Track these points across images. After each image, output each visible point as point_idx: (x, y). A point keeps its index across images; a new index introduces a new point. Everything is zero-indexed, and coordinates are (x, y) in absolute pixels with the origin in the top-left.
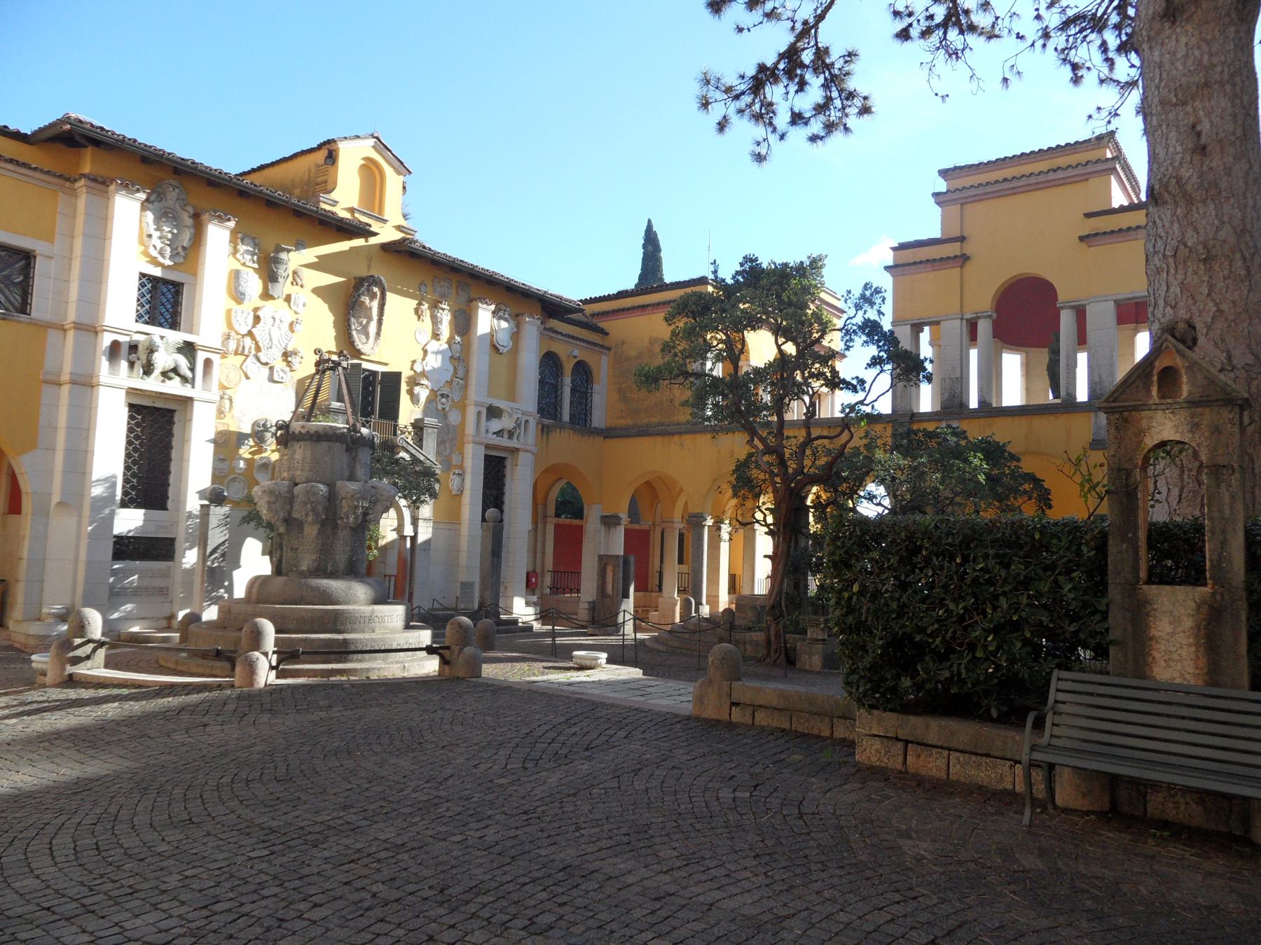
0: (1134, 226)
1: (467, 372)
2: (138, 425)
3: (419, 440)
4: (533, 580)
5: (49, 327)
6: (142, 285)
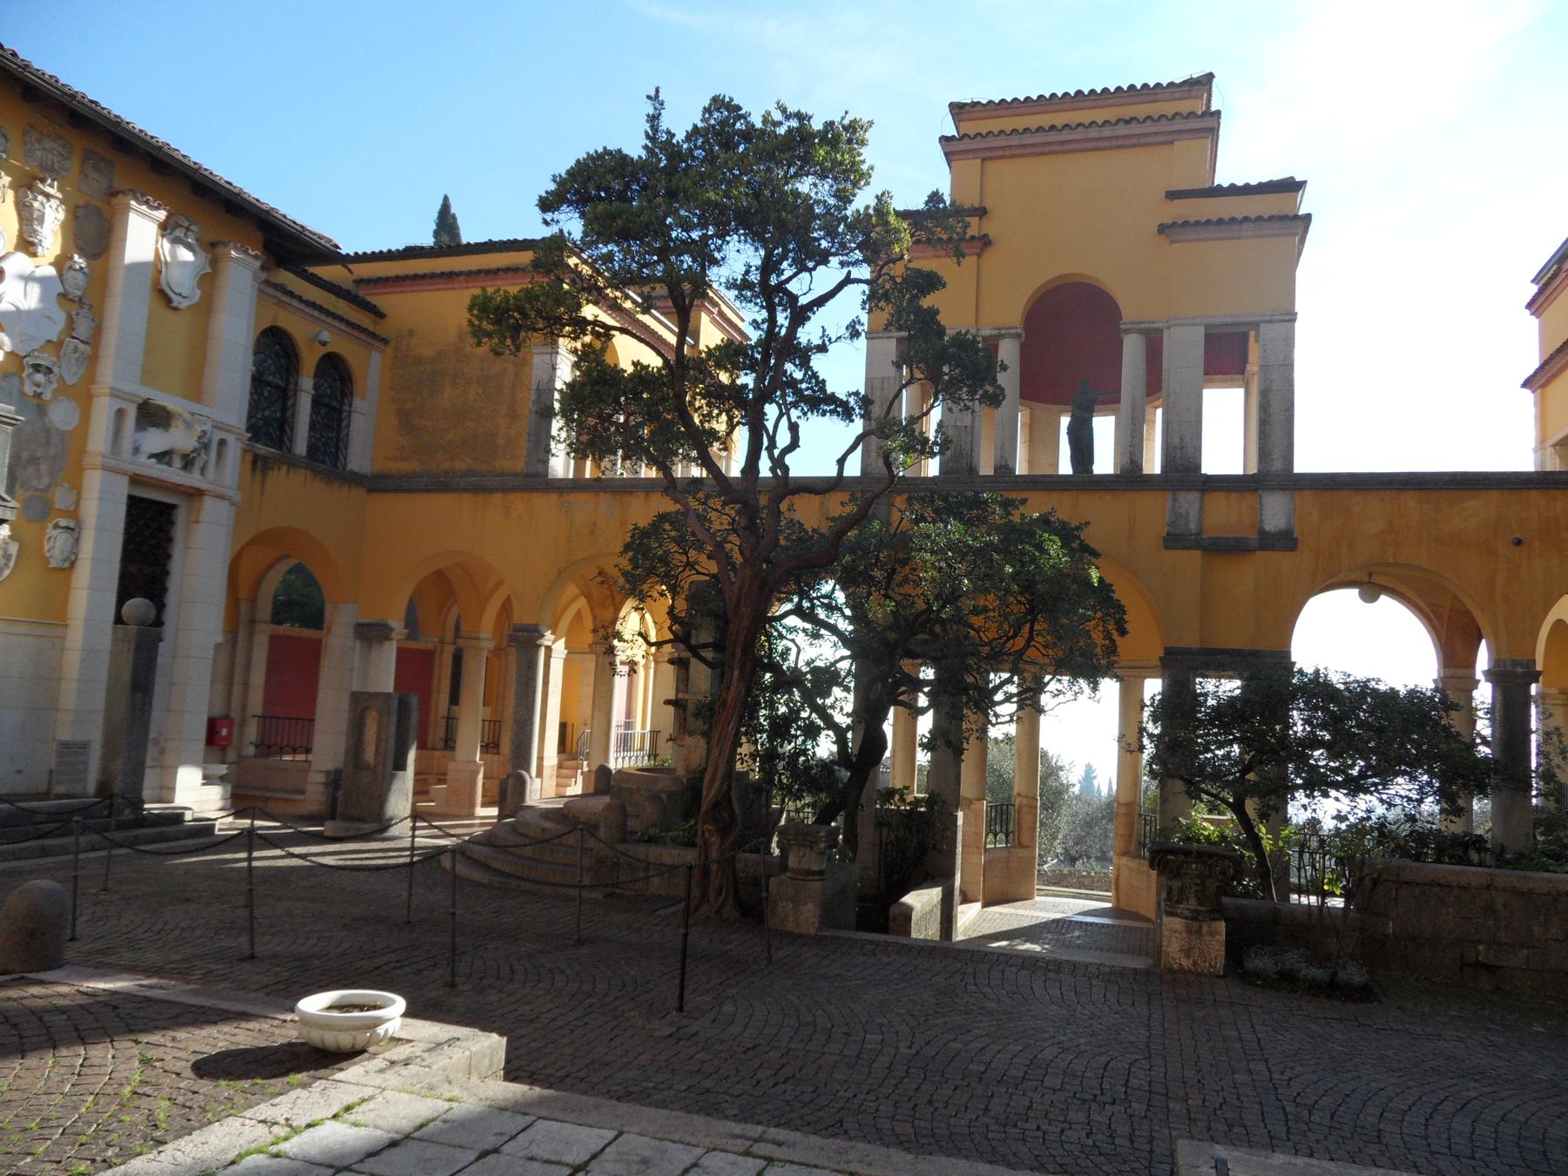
0: (1240, 216)
1: (98, 331)
4: (224, 732)
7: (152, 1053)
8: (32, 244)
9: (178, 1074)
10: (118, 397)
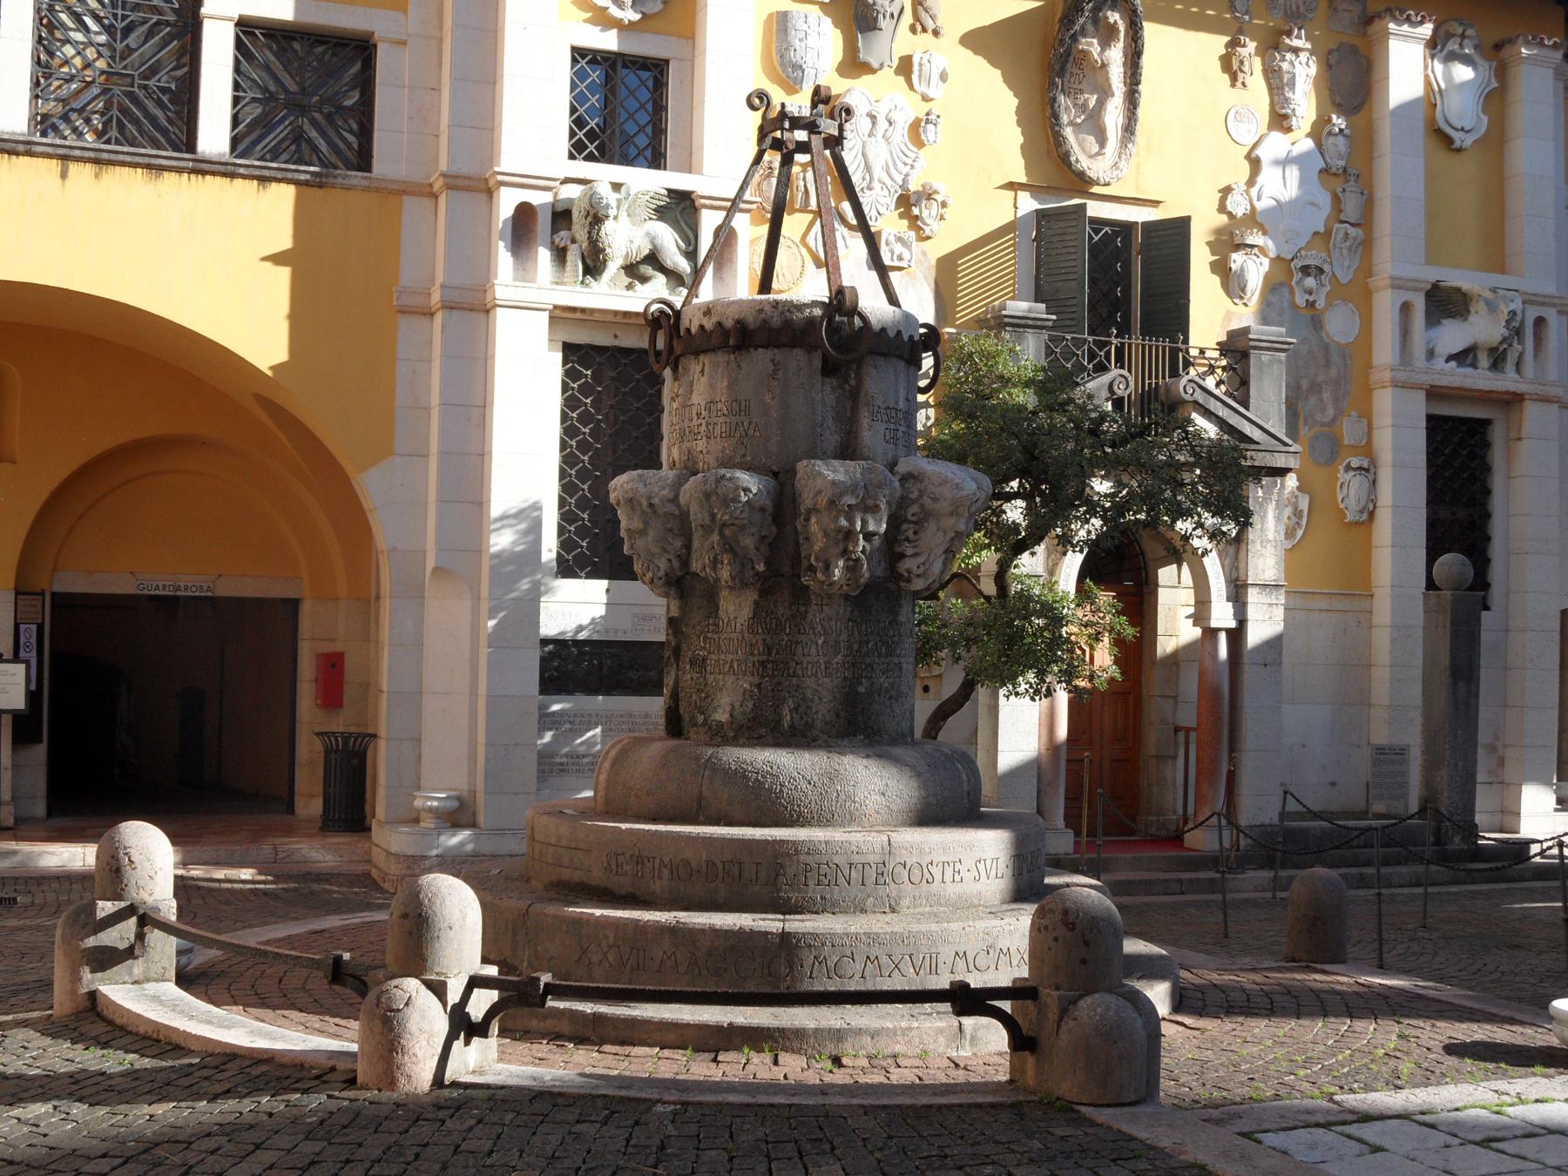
2: (586, 390)
3: (1240, 386)
5: (404, 192)
6: (578, 76)
7: (1409, 1032)
8: (1286, 117)
9: (1428, 1049)
10: (1400, 288)
